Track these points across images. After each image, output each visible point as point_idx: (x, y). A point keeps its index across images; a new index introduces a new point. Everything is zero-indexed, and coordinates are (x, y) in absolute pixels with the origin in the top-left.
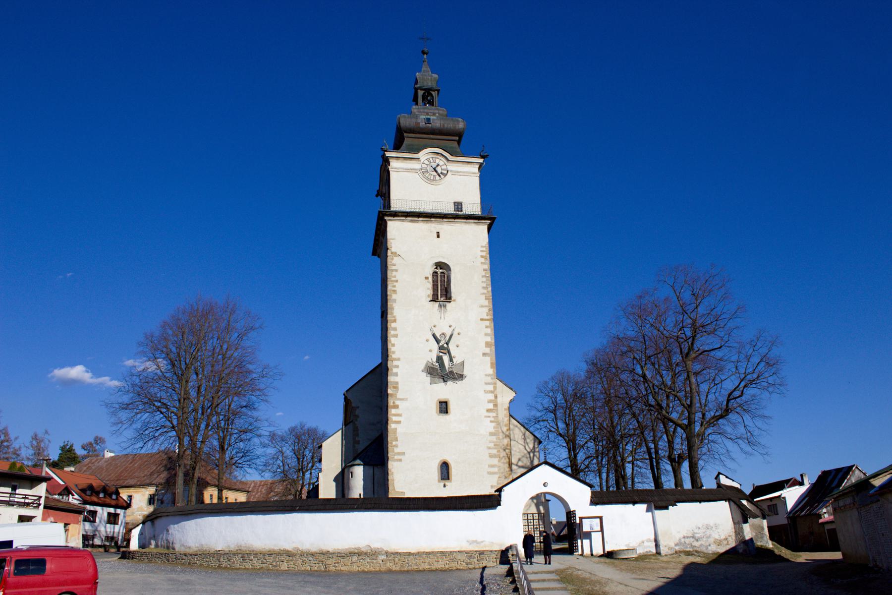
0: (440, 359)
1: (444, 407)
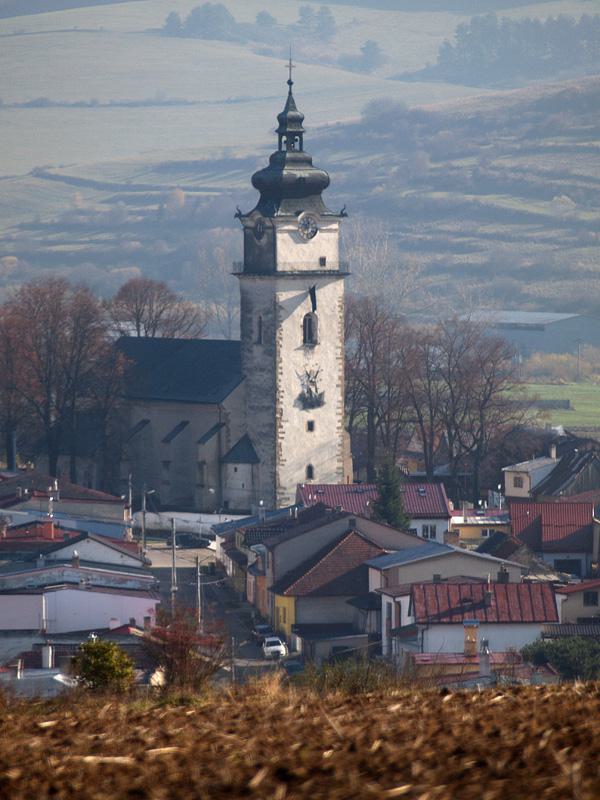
1: (311, 426)
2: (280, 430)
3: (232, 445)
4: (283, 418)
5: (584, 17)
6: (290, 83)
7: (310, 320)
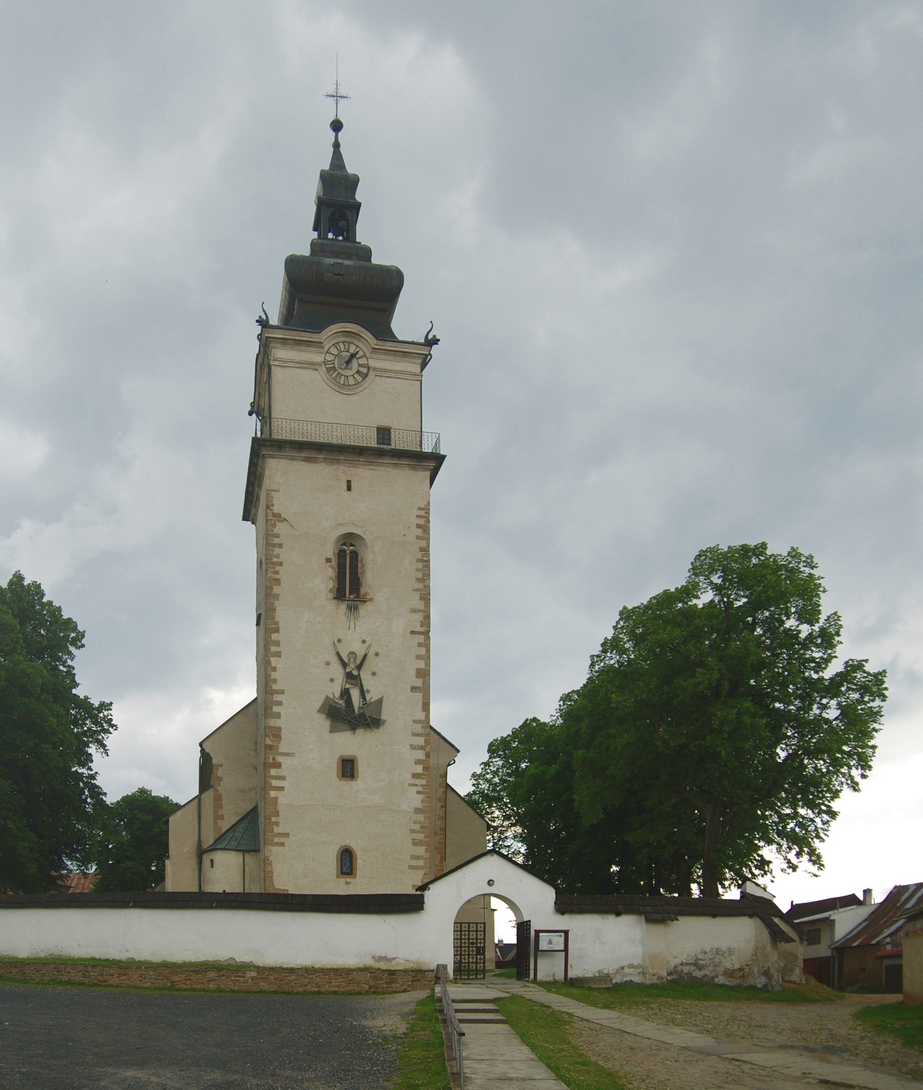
0: (345, 693)
1: (348, 768)
2: (273, 772)
3: (226, 825)
4: (283, 748)
5: (676, 589)
6: (337, 126)
7: (355, 555)
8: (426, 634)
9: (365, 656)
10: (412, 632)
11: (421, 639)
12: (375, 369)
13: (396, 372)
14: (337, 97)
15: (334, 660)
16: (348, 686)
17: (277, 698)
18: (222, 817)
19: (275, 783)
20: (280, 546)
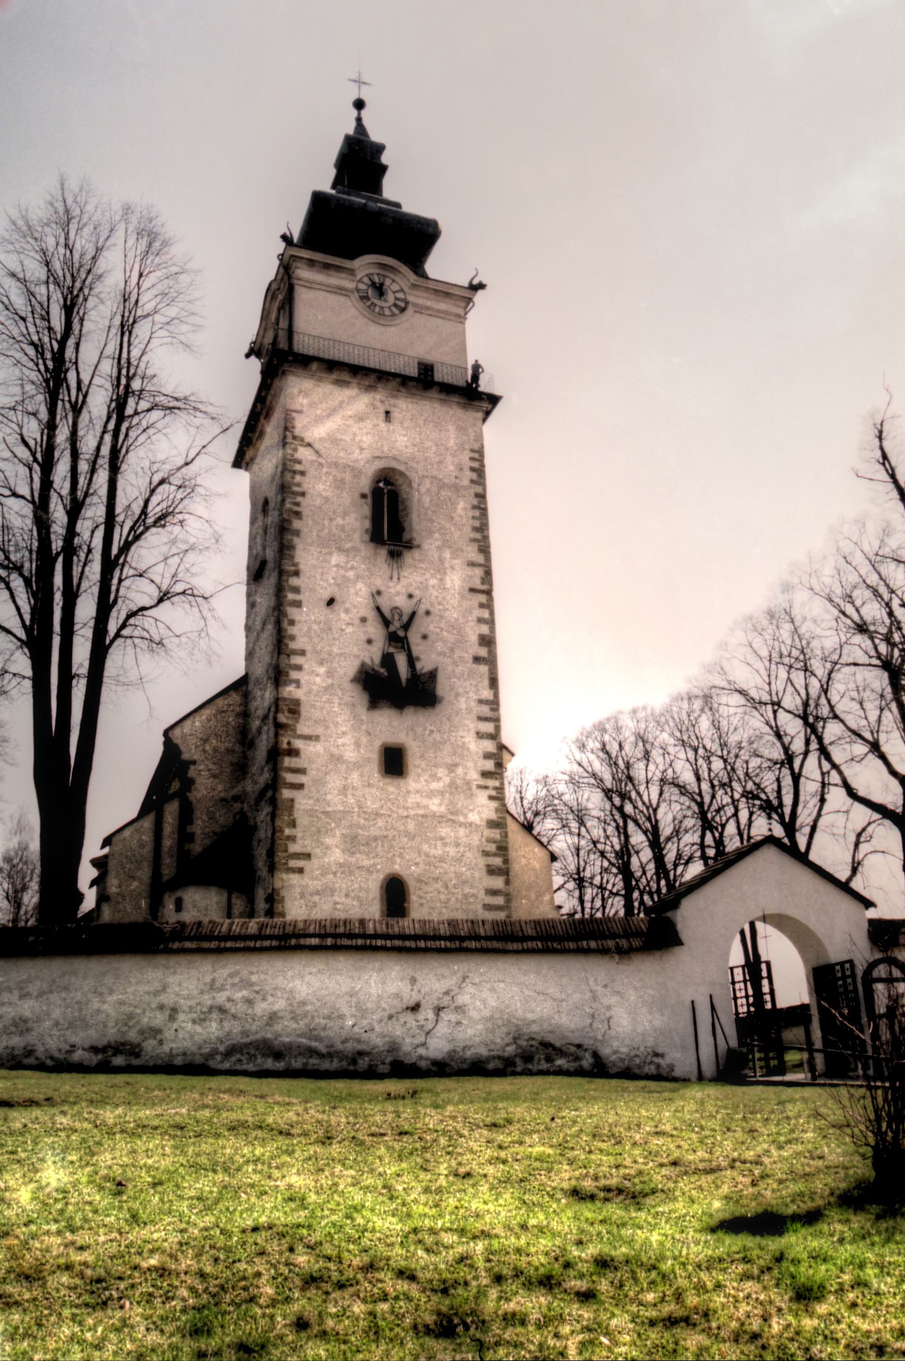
0: (388, 660)
2: (287, 762)
4: (303, 728)
6: (359, 105)
8: (489, 593)
9: (414, 614)
10: (472, 590)
11: (483, 598)
12: (415, 305)
13: (439, 311)
14: (359, 82)
15: (371, 615)
16: (391, 650)
17: (297, 660)
18: (191, 838)
19: (290, 778)
20: (303, 473)
